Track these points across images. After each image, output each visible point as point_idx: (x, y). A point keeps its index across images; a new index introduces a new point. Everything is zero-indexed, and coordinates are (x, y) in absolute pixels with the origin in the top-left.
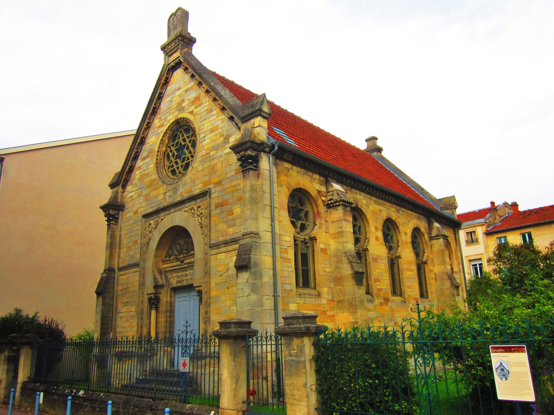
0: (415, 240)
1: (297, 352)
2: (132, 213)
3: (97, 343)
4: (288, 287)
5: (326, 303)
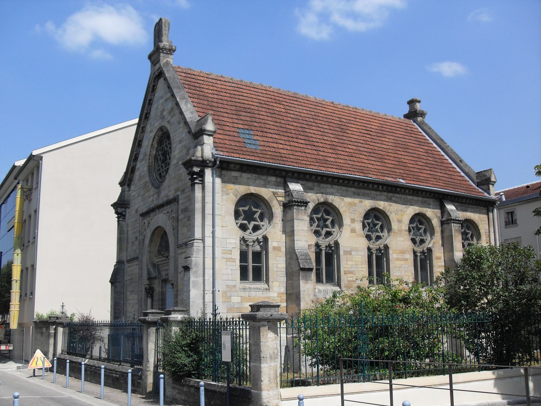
3: (210, 322)
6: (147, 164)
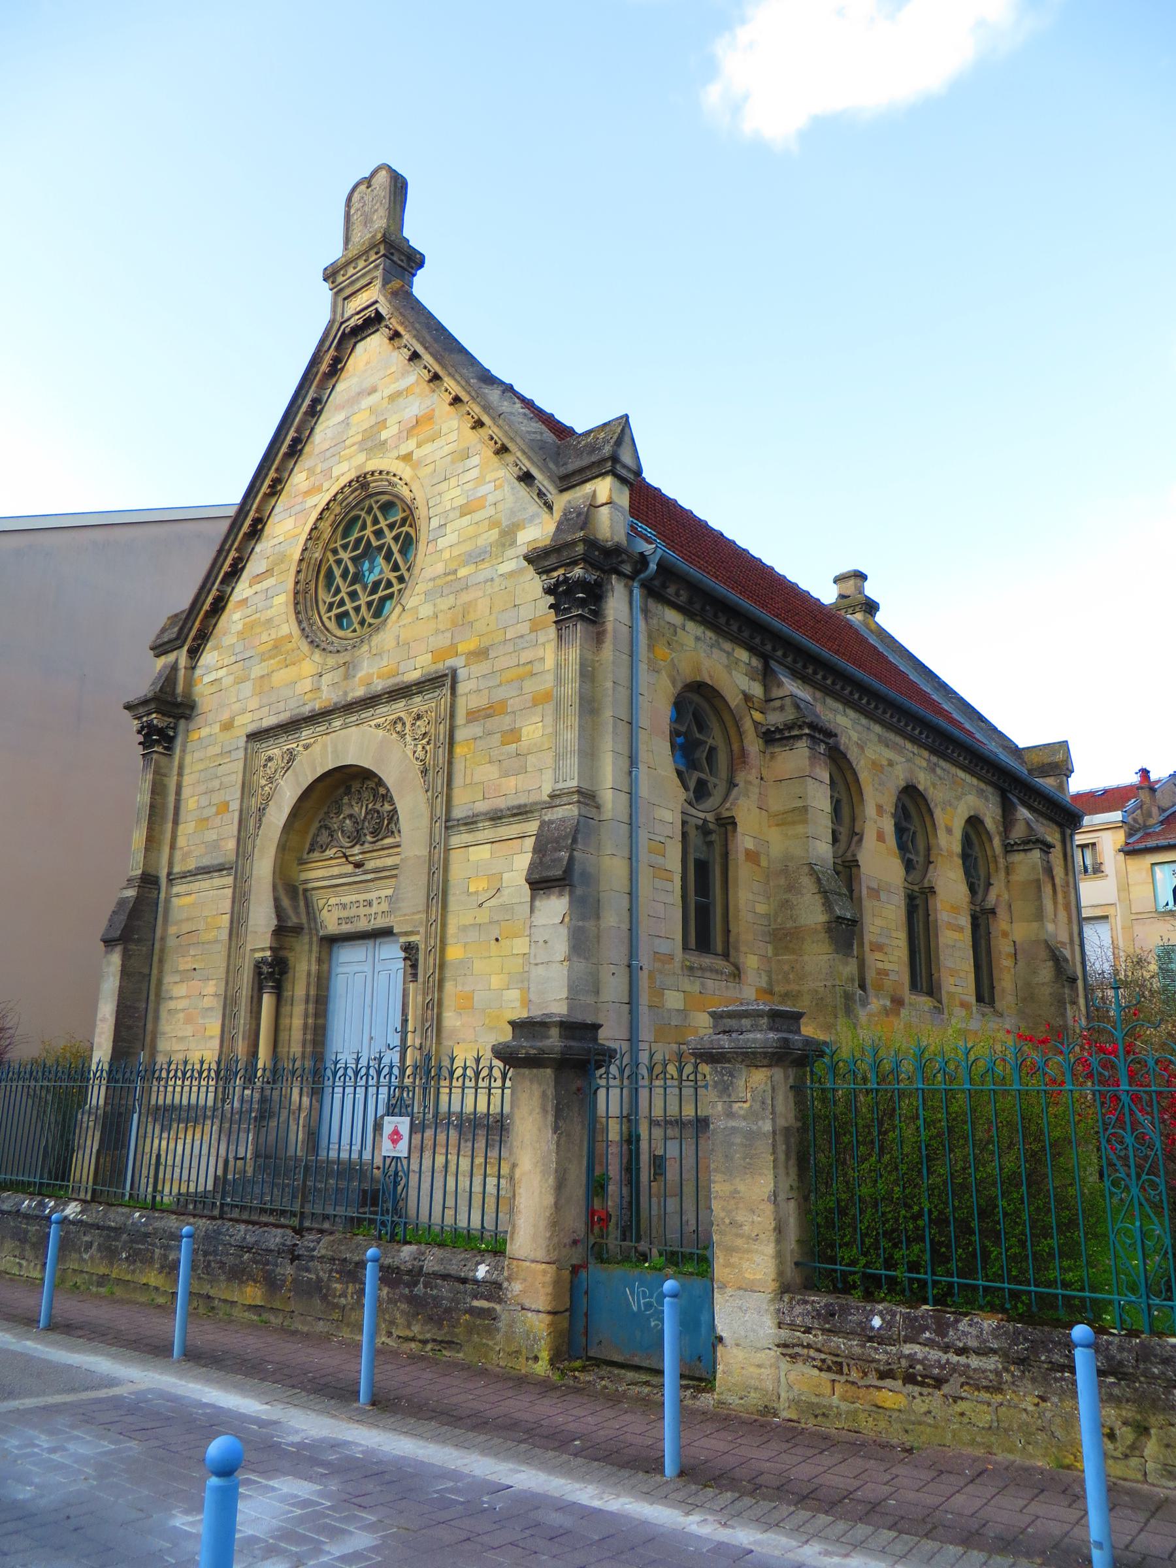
0: (970, 852)
1: (751, 1106)
2: (216, 728)
4: (664, 947)
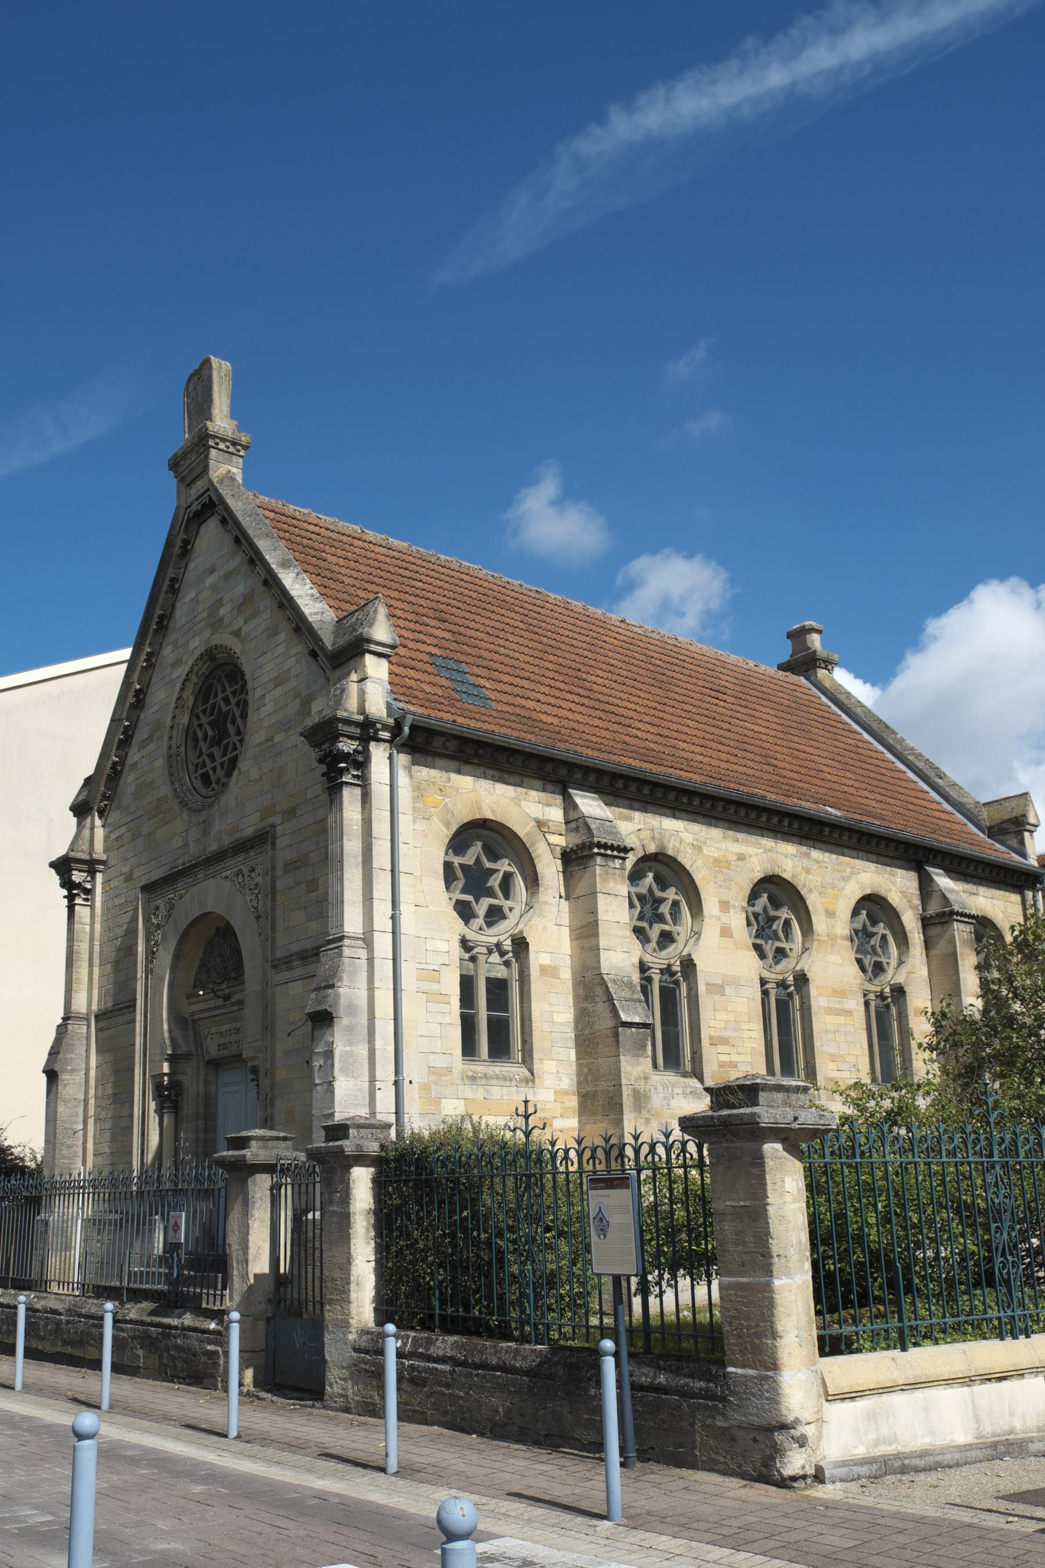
5: (552, 1099)
6: (164, 750)
